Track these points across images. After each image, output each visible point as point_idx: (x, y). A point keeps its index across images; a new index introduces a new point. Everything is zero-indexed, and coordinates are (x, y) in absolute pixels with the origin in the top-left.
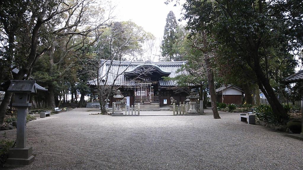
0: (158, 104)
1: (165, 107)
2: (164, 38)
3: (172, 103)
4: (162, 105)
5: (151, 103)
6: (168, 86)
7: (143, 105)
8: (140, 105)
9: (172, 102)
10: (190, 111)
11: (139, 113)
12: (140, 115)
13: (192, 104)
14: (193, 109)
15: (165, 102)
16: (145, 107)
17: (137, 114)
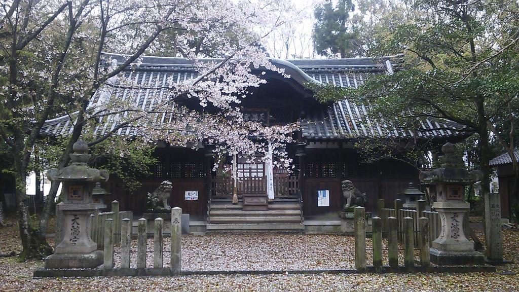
0: (298, 206)
1: (322, 216)
2: (324, 41)
3: (347, 205)
4: (311, 210)
5: (271, 203)
6: (332, 137)
7: (240, 212)
8: (97, 231)
9: (349, 200)
10: (444, 246)
11: (176, 261)
12: (185, 268)
13: (452, 213)
14: (455, 236)
15: (324, 200)
16: (248, 219)
17: (166, 262)
